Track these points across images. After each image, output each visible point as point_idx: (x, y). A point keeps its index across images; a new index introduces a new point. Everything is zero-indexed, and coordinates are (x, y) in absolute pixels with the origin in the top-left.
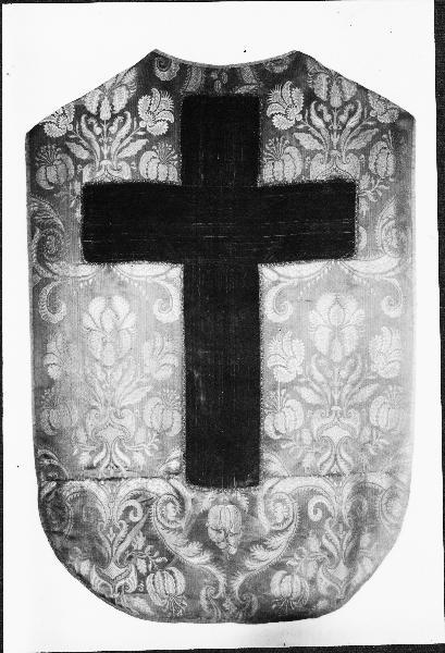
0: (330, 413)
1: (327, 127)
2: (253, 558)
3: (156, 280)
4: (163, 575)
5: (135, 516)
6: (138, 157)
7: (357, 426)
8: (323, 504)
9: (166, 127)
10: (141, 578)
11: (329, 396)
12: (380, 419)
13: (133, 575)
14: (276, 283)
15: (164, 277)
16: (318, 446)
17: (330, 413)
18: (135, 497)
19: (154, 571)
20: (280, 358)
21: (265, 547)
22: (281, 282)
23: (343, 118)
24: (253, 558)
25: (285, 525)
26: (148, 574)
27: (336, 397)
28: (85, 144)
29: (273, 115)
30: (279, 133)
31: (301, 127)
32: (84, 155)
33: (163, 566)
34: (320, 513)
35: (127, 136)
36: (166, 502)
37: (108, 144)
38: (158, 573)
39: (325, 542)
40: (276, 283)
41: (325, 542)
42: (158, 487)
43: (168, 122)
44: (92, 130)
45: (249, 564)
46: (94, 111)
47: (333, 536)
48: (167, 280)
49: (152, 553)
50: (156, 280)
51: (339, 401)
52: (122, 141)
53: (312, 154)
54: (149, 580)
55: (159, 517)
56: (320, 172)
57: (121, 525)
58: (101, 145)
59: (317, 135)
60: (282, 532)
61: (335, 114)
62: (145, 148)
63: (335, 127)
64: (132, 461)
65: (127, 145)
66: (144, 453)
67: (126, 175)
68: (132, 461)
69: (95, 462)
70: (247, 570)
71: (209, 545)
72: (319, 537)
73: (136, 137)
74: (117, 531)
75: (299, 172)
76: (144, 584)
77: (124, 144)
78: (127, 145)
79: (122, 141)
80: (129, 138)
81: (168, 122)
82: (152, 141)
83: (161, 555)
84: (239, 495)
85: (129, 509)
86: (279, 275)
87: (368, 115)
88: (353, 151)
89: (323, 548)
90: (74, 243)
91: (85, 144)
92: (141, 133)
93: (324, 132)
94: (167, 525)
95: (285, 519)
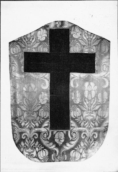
0: (88, 113)
1: (87, 40)
2: (66, 146)
3: (41, 79)
4: (42, 151)
5: (36, 137)
6: (37, 47)
7: (95, 116)
8: (85, 134)
9: (45, 38)
10: (37, 153)
11: (88, 108)
12: (101, 114)
13: (35, 152)
14: (73, 78)
15: (44, 77)
16: (85, 121)
17: (88, 113)
18: (36, 132)
19: (40, 151)
20: (75, 97)
21: (70, 143)
22: (75, 76)
23: (91, 37)
24: (66, 146)
25: (76, 139)
26: (39, 151)
27: (89, 109)
28: (24, 43)
29: (73, 34)
30: (74, 39)
31: (80, 38)
32: (23, 46)
33: (43, 149)
34: (84, 136)
35: (34, 42)
36: (44, 133)
37: (30, 44)
38: (41, 151)
39: (26, 143)
40: (73, 78)
41: (26, 143)
42: (43, 130)
43: (45, 37)
44: (25, 40)
45: (65, 147)
46: (87, 97)
47: (87, 142)
48: (45, 78)
49: (40, 146)
50: (41, 79)
51: (90, 110)
52: (94, 106)
53: (84, 46)
54: (39, 153)
55: (42, 136)
56: (86, 51)
57: (32, 139)
58: (28, 44)
59: (85, 41)
60: (74, 140)
61: (89, 36)
62: (39, 45)
63: (90, 40)
64: (35, 125)
65: (95, 107)
66: (38, 123)
67: (34, 51)
68: (35, 125)
69: (26, 125)
70: (65, 149)
71: (55, 143)
72: (84, 142)
73: (37, 42)
74: (31, 141)
75: (80, 50)
76: (38, 154)
77: (34, 44)
78: (95, 107)
79: (94, 106)
80: (96, 105)
81: (45, 37)
82: (41, 42)
83: (42, 147)
84: (65, 131)
85: (35, 135)
86: (74, 76)
87: (37, 39)
88: (95, 46)
89: (25, 145)
90: (35, 80)
91: (24, 43)
92: (38, 41)
93: (87, 41)
94: (44, 139)
95: (75, 137)
